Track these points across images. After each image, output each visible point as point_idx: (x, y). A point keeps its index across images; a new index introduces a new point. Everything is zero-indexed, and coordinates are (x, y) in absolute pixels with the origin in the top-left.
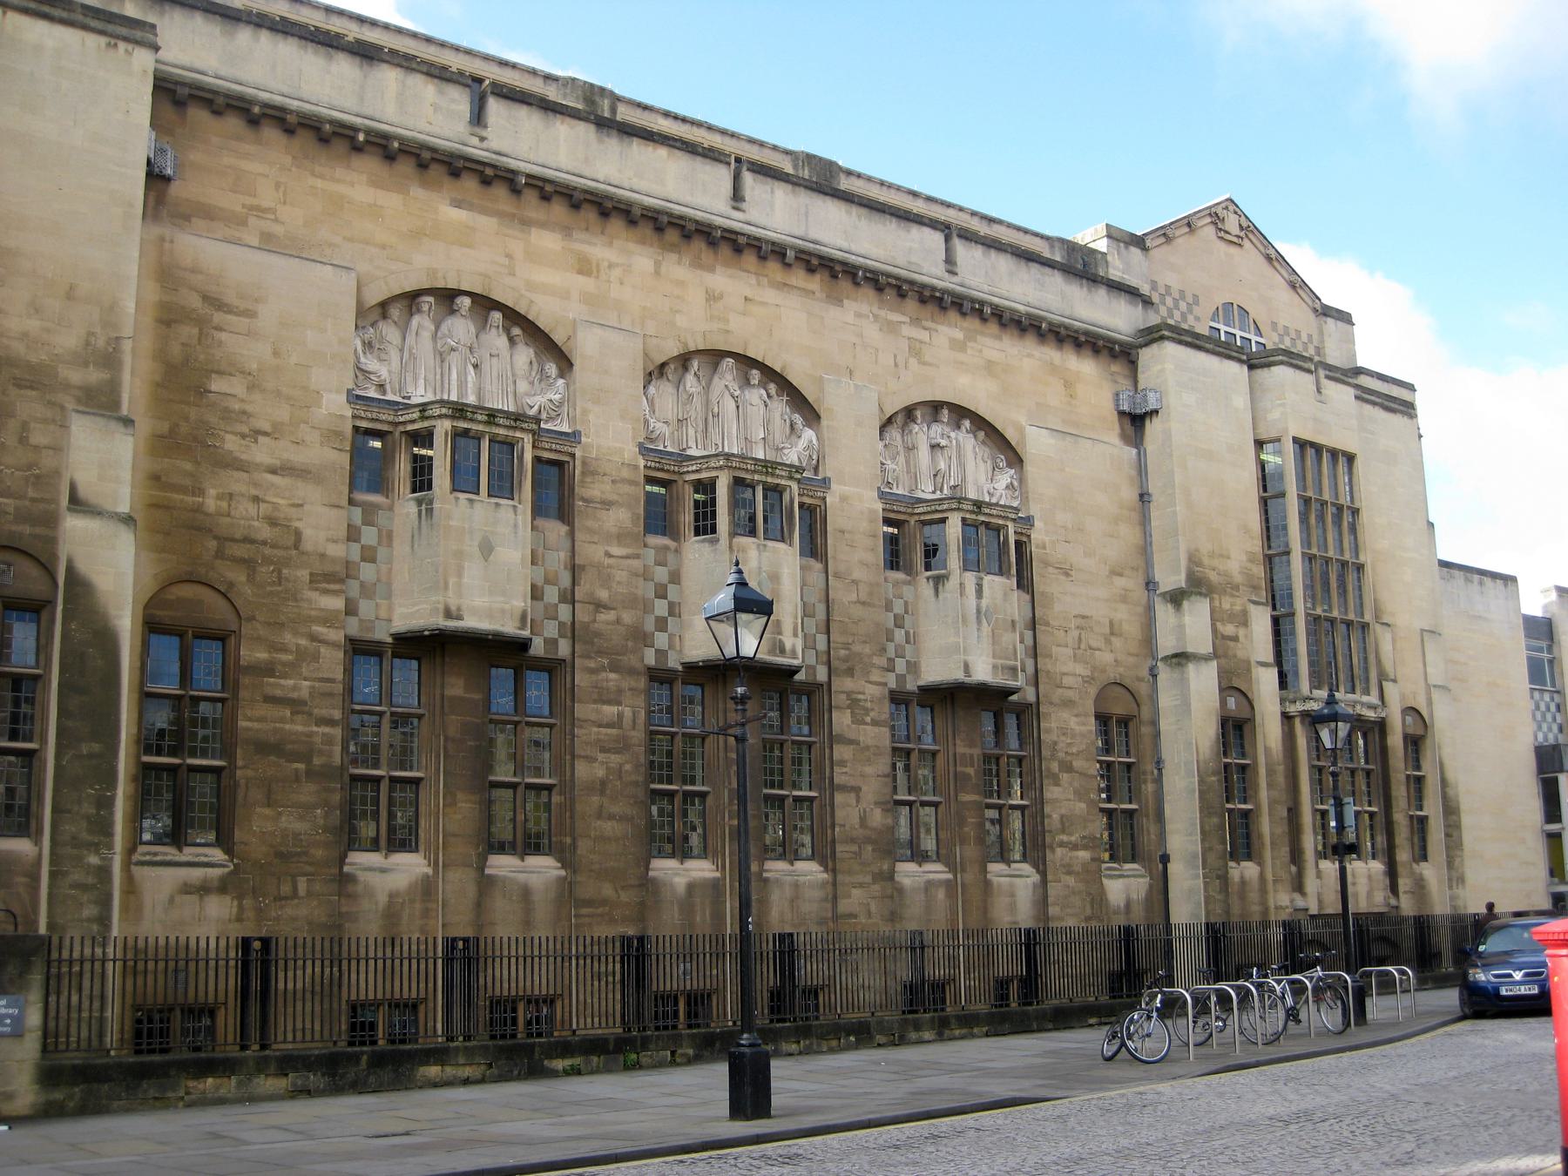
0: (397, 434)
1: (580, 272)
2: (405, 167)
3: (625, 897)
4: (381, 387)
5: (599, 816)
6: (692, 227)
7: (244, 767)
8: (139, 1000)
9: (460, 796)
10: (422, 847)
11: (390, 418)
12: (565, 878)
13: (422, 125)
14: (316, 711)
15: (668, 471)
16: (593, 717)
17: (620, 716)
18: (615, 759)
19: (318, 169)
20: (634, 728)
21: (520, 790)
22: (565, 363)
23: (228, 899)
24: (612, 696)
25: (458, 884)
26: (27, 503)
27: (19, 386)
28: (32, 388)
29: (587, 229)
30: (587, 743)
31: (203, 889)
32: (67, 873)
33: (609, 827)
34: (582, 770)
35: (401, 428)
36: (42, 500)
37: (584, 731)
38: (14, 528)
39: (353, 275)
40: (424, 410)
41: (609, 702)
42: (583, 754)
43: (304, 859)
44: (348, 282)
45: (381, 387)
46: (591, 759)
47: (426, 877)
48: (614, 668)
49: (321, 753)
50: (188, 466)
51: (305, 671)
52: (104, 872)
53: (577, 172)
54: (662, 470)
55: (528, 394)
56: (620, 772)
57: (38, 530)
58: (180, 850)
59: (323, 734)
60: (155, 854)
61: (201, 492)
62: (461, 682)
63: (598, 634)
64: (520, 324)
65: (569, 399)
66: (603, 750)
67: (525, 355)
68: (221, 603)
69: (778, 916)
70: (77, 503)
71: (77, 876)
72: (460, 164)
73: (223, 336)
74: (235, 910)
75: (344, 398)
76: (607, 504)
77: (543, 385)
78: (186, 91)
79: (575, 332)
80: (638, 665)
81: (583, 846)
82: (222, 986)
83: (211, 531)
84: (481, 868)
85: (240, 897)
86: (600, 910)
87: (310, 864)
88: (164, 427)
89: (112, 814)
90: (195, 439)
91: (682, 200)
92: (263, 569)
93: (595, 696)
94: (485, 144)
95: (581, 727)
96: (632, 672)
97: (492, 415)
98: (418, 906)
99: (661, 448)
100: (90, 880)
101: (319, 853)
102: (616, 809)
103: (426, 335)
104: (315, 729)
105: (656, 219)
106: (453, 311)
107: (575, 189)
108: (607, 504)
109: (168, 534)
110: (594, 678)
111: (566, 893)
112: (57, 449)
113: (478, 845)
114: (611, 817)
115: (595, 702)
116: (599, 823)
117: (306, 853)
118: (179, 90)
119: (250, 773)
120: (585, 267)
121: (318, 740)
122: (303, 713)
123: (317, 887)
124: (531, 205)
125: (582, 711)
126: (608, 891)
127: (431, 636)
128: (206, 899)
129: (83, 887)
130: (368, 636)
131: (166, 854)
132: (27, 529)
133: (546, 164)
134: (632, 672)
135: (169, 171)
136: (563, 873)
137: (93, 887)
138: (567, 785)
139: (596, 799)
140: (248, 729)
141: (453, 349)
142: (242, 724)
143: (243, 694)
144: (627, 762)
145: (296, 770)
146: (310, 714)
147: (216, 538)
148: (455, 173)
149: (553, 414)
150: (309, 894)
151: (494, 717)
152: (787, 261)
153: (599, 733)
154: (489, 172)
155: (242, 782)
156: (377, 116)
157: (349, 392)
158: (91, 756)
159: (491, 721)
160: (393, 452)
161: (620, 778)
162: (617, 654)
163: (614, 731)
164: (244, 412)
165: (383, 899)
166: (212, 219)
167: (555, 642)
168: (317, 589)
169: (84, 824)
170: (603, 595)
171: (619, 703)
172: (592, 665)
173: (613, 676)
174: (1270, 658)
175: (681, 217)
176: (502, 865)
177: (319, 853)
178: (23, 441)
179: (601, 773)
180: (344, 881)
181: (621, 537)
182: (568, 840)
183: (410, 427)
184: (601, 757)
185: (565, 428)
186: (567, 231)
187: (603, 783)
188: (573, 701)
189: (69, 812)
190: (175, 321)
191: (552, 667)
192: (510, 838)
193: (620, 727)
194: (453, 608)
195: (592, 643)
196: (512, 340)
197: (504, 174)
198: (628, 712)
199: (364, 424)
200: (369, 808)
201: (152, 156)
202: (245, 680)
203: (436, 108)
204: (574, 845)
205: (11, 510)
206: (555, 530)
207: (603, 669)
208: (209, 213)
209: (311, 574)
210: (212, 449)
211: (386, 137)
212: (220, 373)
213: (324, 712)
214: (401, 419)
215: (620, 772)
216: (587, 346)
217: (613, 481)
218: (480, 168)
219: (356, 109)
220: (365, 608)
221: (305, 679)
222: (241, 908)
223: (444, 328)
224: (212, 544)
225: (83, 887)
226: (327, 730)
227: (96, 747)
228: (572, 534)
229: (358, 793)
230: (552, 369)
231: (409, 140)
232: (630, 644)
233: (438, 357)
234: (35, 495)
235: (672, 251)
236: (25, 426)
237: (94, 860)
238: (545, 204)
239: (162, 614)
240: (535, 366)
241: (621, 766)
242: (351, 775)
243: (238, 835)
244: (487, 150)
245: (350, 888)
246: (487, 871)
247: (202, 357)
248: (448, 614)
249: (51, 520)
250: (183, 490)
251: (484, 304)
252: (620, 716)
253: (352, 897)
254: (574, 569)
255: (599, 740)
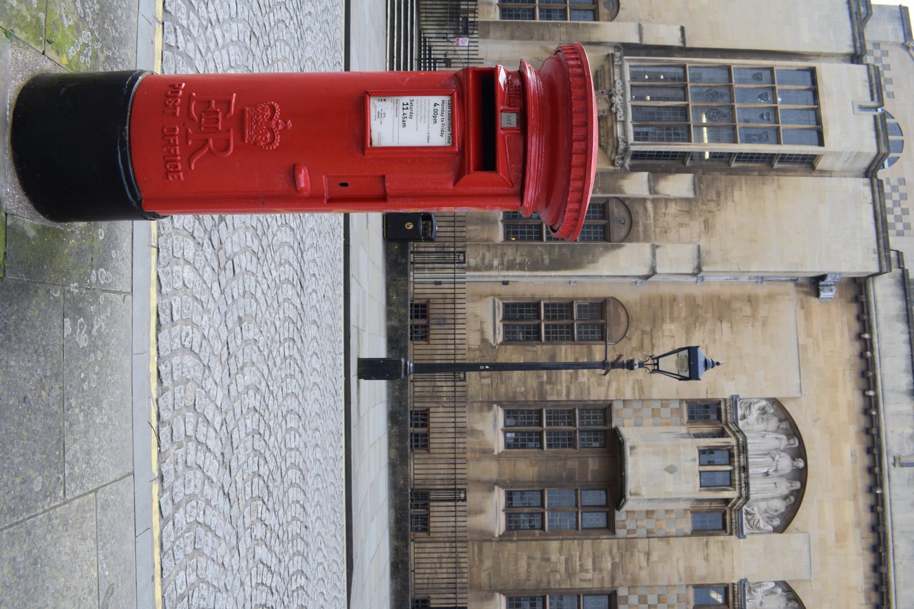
0: (721, 425)
1: (837, 535)
2: (863, 421)
3: (484, 575)
4: (744, 417)
5: (529, 557)
6: (881, 530)
7: (542, 350)
8: (431, 301)
9: (536, 469)
10: (507, 450)
11: (729, 420)
12: (494, 537)
13: (889, 429)
14: (573, 386)
15: (734, 600)
16: (585, 553)
17: (587, 571)
18: (562, 567)
19: (847, 372)
20: (581, 580)
21: (541, 510)
22: (780, 529)
23: (479, 343)
24: (597, 565)
25: (489, 469)
26: (653, 228)
27: (705, 222)
28: (705, 227)
29: (863, 538)
30: (569, 550)
31: (482, 332)
32: (489, 251)
33: (523, 564)
34: (554, 545)
35: (725, 427)
36: (656, 236)
37: (576, 546)
38: (641, 224)
39: (799, 395)
40: (737, 432)
41: (594, 563)
42: (564, 545)
43: (499, 382)
44: (794, 392)
45: (744, 417)
46: (561, 551)
47: (493, 535)
48: (614, 565)
49: (553, 389)
50: (683, 315)
51: (592, 379)
52: (490, 267)
53: (894, 526)
54: (734, 596)
55: (759, 508)
56: (555, 571)
57: (641, 234)
58: (503, 511)
59: (562, 390)
60: (499, 309)
61: (672, 319)
62: (596, 468)
63: (632, 555)
64: (796, 499)
65: (761, 531)
66: (567, 560)
67: (780, 506)
68: (621, 334)
69: (474, 497)
70: (654, 248)
71: (488, 256)
72: (875, 451)
73: (750, 328)
74: (473, 347)
75: (734, 393)
76: (706, 558)
77: (766, 519)
78: (864, 300)
79: (801, 533)
80: (617, 583)
81: (511, 547)
82: (440, 7)
83: (654, 327)
84: (497, 483)
85: (480, 350)
86: (476, 558)
87: (497, 385)
88: (699, 302)
89: (517, 270)
90: (697, 317)
91: (899, 601)
92: (640, 355)
93: (597, 554)
94: (891, 466)
95: (578, 545)
96: (613, 579)
97: (745, 469)
98: (477, 447)
99: (747, 598)
100: (487, 261)
101: (502, 389)
102: (534, 568)
103: (776, 443)
104: (564, 385)
105: (882, 584)
106: (793, 459)
107: (884, 526)
108: (706, 558)
109: (649, 307)
110: (607, 552)
111: (485, 537)
112: (679, 241)
113: (510, 480)
114: (529, 565)
115: (594, 554)
116: (525, 557)
117: (502, 383)
118: (863, 296)
119: (540, 352)
120: (840, 538)
121: (559, 387)
122: (572, 379)
123: (486, 389)
124: (864, 501)
125: (587, 543)
126: (488, 563)
127: (620, 441)
128: (479, 333)
129: (483, 258)
130: (614, 415)
131: (499, 314)
132: (641, 229)
133: (893, 506)
134: (613, 579)
135: (823, 295)
136: (497, 535)
137: (484, 263)
138: (545, 538)
139: (538, 555)
140: (561, 350)
141: (773, 458)
142: (563, 348)
143: (578, 347)
144: (561, 576)
145: (543, 376)
146: (571, 383)
147: (651, 330)
148: (869, 451)
149: (751, 522)
150: (482, 385)
151: (579, 492)
152: (873, 489)
153: (576, 556)
154: (877, 470)
155: (535, 349)
156: (885, 401)
157: (746, 580)
158: (543, 260)
159: (576, 490)
160: (712, 424)
161: (552, 571)
162: (622, 567)
163: (578, 567)
164: (715, 341)
165: (479, 427)
166: (806, 319)
167: (624, 527)
168: (634, 384)
169: (511, 258)
170: (654, 557)
171: (594, 570)
172: (615, 550)
173: (609, 566)
174: (649, 40)
175: (889, 601)
176: (499, 496)
177: (502, 389)
178: (681, 225)
179: (554, 558)
180: (488, 404)
181: (690, 569)
182: (515, 538)
183: (727, 430)
184: (563, 558)
185: (745, 531)
186: (858, 524)
187: (548, 560)
188: (592, 539)
189: (517, 251)
190: (751, 304)
191: (610, 527)
192: (514, 505)
193: (580, 572)
194: (636, 450)
195: (626, 551)
196: (786, 498)
197: (878, 480)
198: (589, 576)
199: (723, 407)
200: (526, 230)
201: (829, 280)
202: (585, 348)
203: (902, 434)
204: (511, 541)
205: (648, 222)
206: (686, 525)
207: (613, 558)
208: (808, 317)
209: (641, 380)
210: (693, 326)
211: (877, 407)
212: (732, 327)
213: (573, 390)
214: (730, 425)
215: (555, 571)
216: (792, 539)
217: (721, 562)
218: (877, 464)
219: (886, 388)
220: (628, 412)
221: (588, 379)
222: (475, 350)
223: (783, 454)
224: (648, 329)
225: (483, 258)
226: (564, 392)
227: (547, 262)
228: (686, 536)
229: (534, 415)
230: (777, 522)
231: (879, 420)
232: (629, 576)
233: (767, 452)
234: (657, 233)
235: (866, 598)
236: (687, 225)
237: (496, 263)
238: (869, 510)
239: (610, 308)
240: (775, 514)
241: (559, 572)
242: (544, 490)
243: (510, 347)
244: (888, 468)
245: (485, 408)
246: (496, 487)
247: (737, 318)
248: (632, 448)
249: (646, 239)
250: (672, 313)
251: (801, 475)
252: (587, 571)
253: (481, 410)
254: (667, 537)
255: (572, 557)
